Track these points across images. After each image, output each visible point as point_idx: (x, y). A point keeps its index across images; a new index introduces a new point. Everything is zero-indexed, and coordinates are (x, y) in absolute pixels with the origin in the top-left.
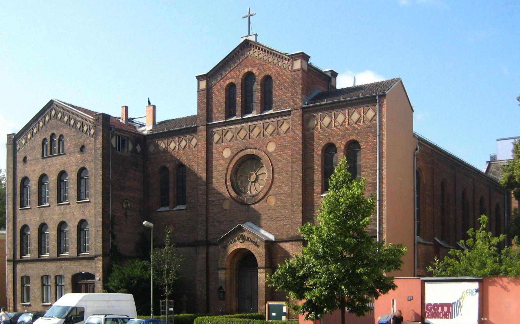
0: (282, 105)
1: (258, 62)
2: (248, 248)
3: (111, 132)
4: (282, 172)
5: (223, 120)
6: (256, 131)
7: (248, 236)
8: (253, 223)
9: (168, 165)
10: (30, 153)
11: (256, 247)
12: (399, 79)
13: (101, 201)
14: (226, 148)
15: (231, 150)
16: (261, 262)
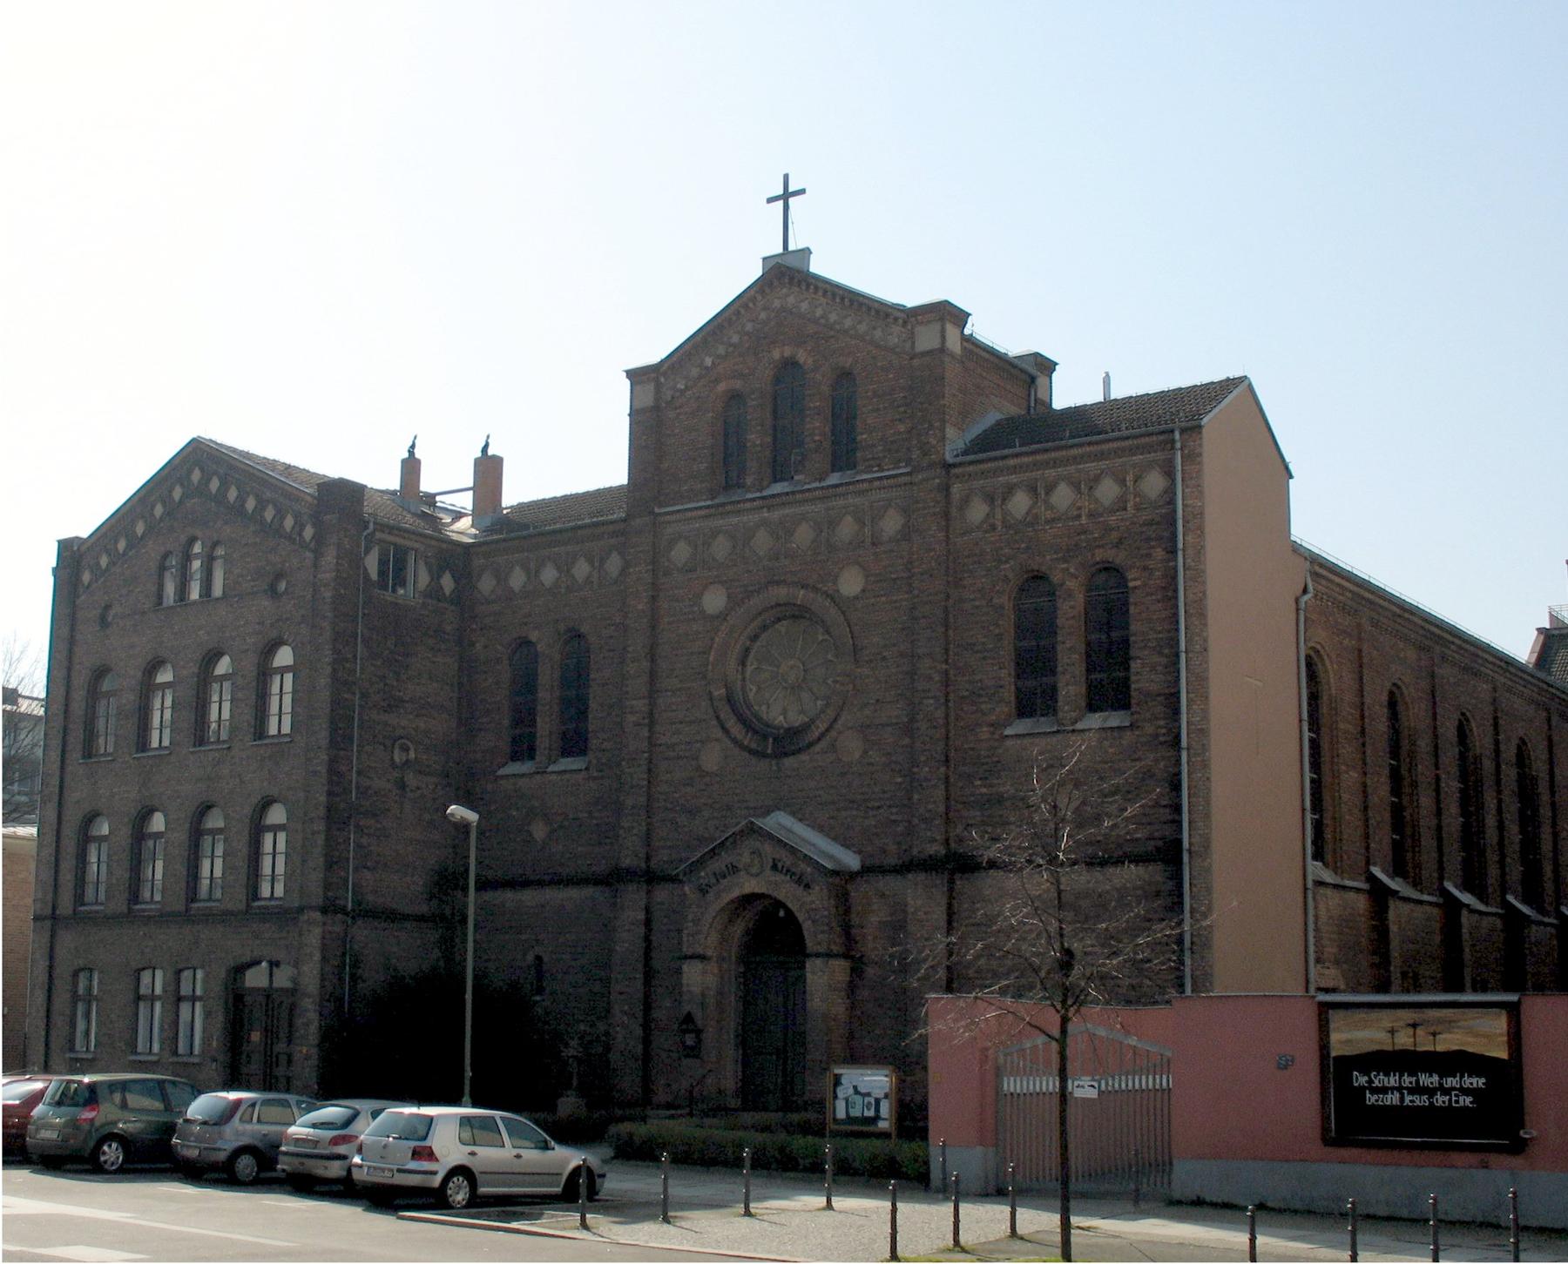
0: (885, 457)
1: (811, 329)
2: (775, 894)
3: (365, 534)
4: (884, 658)
5: (705, 500)
6: (804, 535)
7: (778, 856)
8: (793, 814)
9: (534, 636)
10: (120, 596)
11: (800, 891)
12: (1243, 379)
13: (324, 743)
16: (816, 936)
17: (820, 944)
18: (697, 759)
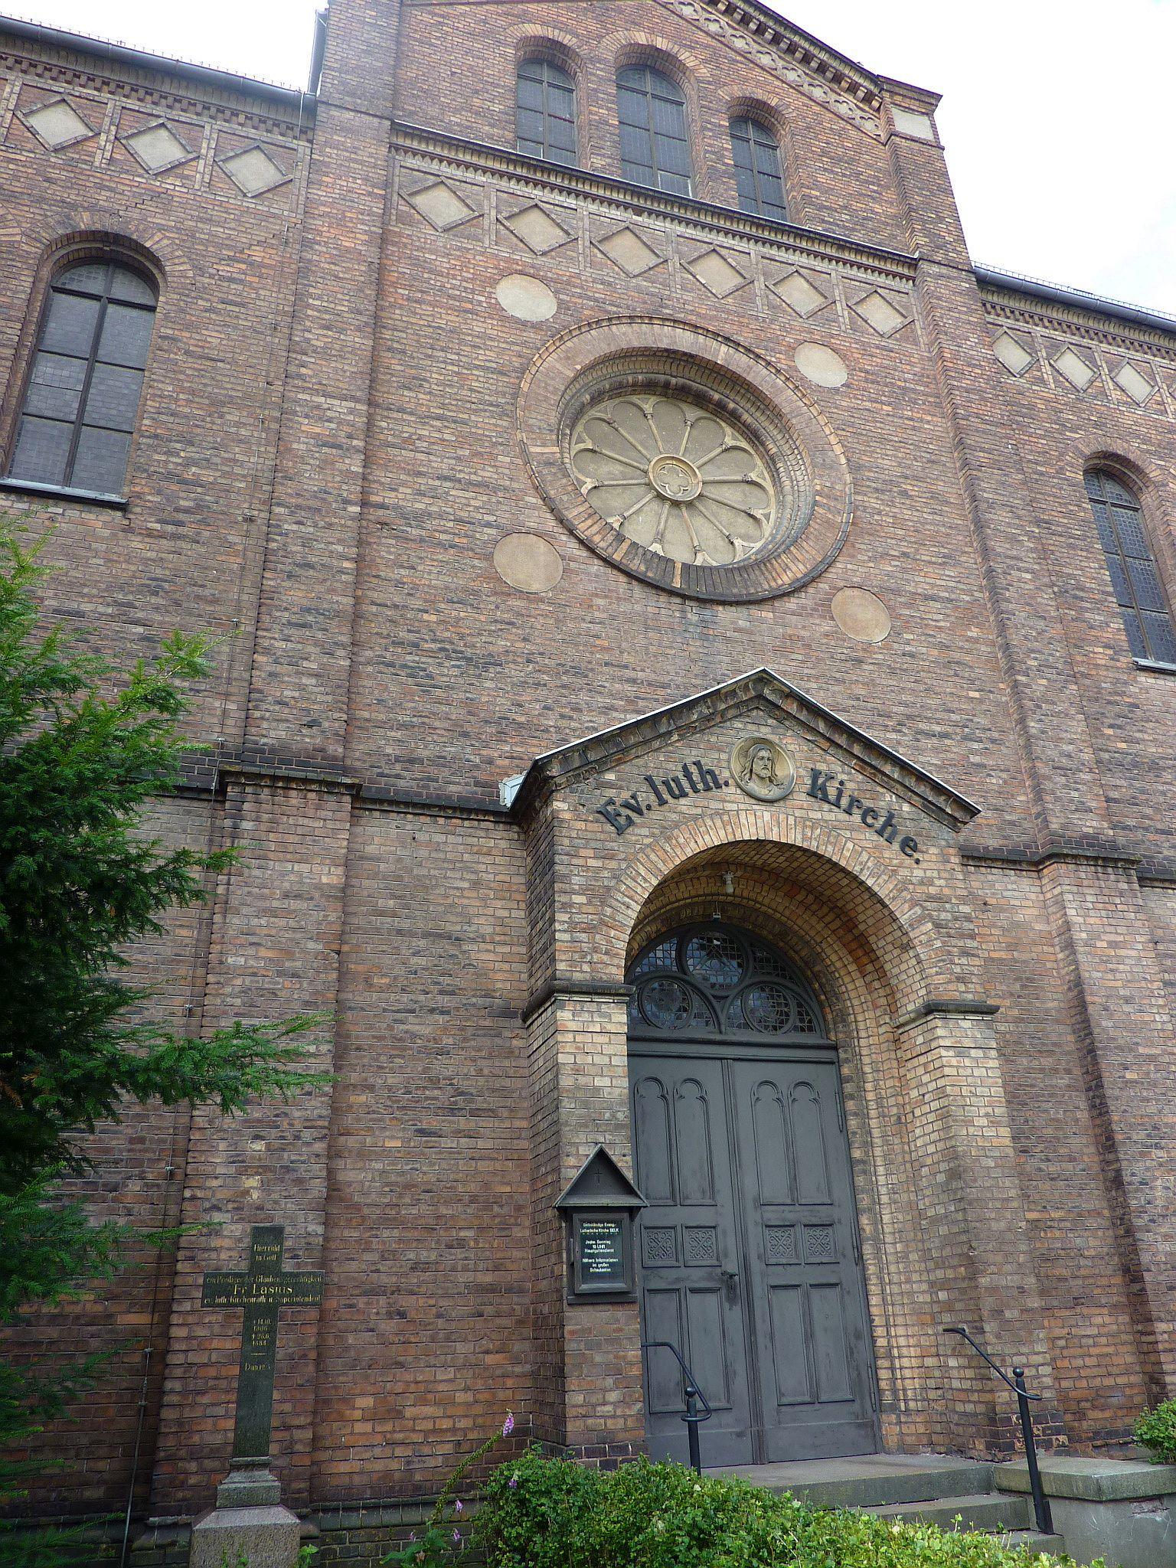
2: (828, 851)
11: (892, 853)
14: (522, 273)
15: (556, 292)
17: (960, 979)
18: (489, 557)
